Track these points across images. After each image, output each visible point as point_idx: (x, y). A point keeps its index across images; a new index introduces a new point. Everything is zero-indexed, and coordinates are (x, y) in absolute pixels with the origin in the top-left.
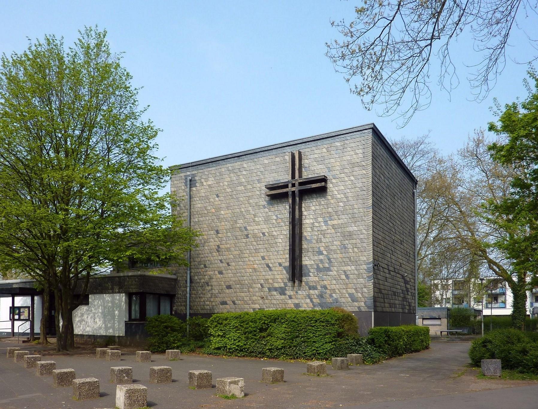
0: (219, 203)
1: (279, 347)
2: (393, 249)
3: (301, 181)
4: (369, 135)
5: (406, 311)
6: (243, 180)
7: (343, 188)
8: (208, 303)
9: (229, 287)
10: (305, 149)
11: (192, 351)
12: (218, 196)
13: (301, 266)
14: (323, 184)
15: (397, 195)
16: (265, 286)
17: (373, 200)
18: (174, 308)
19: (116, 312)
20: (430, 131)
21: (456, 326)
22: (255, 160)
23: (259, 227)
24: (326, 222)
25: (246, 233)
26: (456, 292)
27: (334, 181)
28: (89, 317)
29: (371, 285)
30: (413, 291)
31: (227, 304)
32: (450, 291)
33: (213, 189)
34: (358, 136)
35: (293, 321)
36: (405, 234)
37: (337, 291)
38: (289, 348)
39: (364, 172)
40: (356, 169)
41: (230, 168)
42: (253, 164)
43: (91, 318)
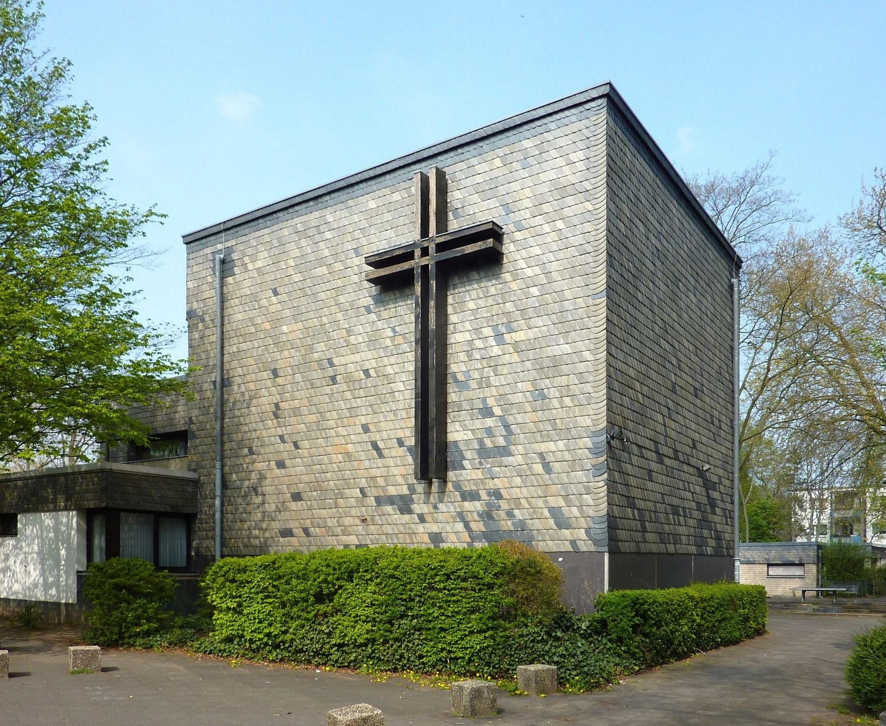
0: (279, 307)
1: (360, 641)
2: (671, 405)
3: (442, 240)
4: (598, 118)
5: (709, 551)
6: (326, 253)
7: (537, 250)
8: (257, 532)
9: (297, 497)
10: (454, 167)
11: (181, 643)
12: (276, 293)
13: (443, 446)
14: (490, 242)
15: (684, 280)
16: (369, 494)
17: (609, 277)
18: (194, 544)
19: (63, 552)
20: (772, 154)
21: (834, 578)
22: (350, 203)
23: (357, 357)
24: (499, 336)
25: (330, 372)
26: (836, 515)
27: (518, 236)
28: (18, 562)
29: (600, 485)
30: (729, 506)
31: (292, 535)
32: (828, 511)
33: (268, 278)
34: (573, 118)
35: (393, 576)
36: (706, 375)
37: (523, 502)
38: (384, 644)
39: (589, 206)
40: (570, 200)
41: (300, 227)
42: (345, 213)
43: (21, 562)
